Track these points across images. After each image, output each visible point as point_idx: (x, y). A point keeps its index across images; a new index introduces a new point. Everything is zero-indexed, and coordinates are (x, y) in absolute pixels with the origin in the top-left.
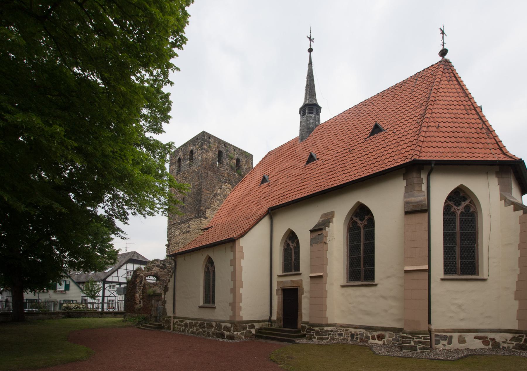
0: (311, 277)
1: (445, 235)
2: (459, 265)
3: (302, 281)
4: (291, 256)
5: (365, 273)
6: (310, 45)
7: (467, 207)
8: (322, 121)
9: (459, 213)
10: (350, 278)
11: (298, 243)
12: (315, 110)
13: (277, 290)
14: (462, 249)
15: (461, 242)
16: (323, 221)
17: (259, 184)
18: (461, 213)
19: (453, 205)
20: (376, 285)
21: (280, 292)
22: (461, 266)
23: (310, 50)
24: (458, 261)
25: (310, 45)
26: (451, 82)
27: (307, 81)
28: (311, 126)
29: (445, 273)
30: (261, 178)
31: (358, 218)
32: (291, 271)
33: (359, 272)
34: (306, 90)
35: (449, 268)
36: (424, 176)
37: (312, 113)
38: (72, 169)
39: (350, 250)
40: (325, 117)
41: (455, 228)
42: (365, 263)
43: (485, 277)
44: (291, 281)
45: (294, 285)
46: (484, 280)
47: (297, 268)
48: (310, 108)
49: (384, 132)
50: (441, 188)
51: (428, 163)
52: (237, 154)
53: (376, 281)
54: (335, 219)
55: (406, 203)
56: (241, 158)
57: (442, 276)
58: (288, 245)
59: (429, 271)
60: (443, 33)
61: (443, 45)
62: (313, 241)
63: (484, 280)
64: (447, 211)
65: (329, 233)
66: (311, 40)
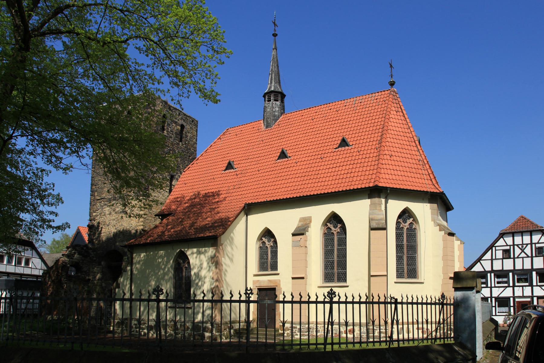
0: (293, 278)
1: (397, 246)
2: (406, 271)
3: (280, 281)
5: (338, 275)
6: (275, 30)
9: (405, 228)
12: (280, 98)
14: (408, 257)
16: (302, 224)
17: (224, 168)
18: (407, 229)
24: (405, 267)
26: (398, 114)
29: (398, 277)
30: (226, 165)
31: (332, 225)
32: (267, 270)
33: (333, 274)
35: (400, 274)
37: (277, 101)
39: (325, 253)
41: (403, 240)
42: (338, 266)
43: (422, 281)
44: (269, 280)
45: (271, 285)
46: (422, 283)
47: (274, 267)
49: (350, 147)
51: (386, 188)
52: (181, 119)
53: (349, 282)
54: (312, 224)
55: (370, 220)
56: (185, 124)
57: (396, 280)
59: (387, 276)
60: (391, 66)
62: (295, 245)
63: (422, 283)
64: (398, 228)
65: (308, 237)
66: (275, 25)
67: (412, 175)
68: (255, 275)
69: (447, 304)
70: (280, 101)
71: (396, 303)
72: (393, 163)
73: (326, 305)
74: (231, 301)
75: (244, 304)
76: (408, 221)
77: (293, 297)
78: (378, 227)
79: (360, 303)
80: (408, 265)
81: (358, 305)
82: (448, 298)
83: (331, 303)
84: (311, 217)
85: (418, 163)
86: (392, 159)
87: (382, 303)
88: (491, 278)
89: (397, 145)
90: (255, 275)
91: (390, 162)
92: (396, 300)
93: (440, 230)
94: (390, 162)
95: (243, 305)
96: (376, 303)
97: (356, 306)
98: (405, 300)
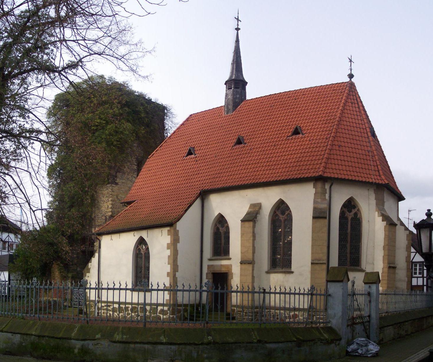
3: (231, 265)
4: (221, 240)
6: (238, 25)
7: (356, 214)
8: (248, 97)
10: (272, 266)
11: (228, 228)
13: (207, 274)
15: (351, 241)
19: (346, 211)
20: (292, 272)
21: (210, 276)
22: (350, 260)
23: (238, 29)
25: (238, 25)
27: (234, 56)
28: (237, 100)
34: (233, 64)
36: (327, 187)
37: (238, 88)
38: (6, 118)
40: (251, 93)
48: (237, 84)
50: (339, 197)
58: (218, 229)
60: (351, 61)
61: (351, 70)
67: (360, 166)
68: (210, 260)
69: (316, 295)
70: (240, 88)
71: (264, 292)
72: (341, 153)
73: (276, 295)
74: (183, 291)
75: (323, 297)
76: (353, 210)
77: (158, 286)
78: (320, 215)
79: (304, 294)
80: (351, 253)
81: (274, 295)
82: (318, 289)
83: (312, 295)
84: (141, 236)
85: (367, 154)
86: (341, 149)
87: (288, 293)
88: (10, 286)
89: (348, 136)
90: (210, 260)
91: (338, 153)
92: (265, 290)
93: (383, 221)
94: (338, 153)
95: (262, 295)
96: (273, 293)
97: (297, 296)
98: (273, 290)
